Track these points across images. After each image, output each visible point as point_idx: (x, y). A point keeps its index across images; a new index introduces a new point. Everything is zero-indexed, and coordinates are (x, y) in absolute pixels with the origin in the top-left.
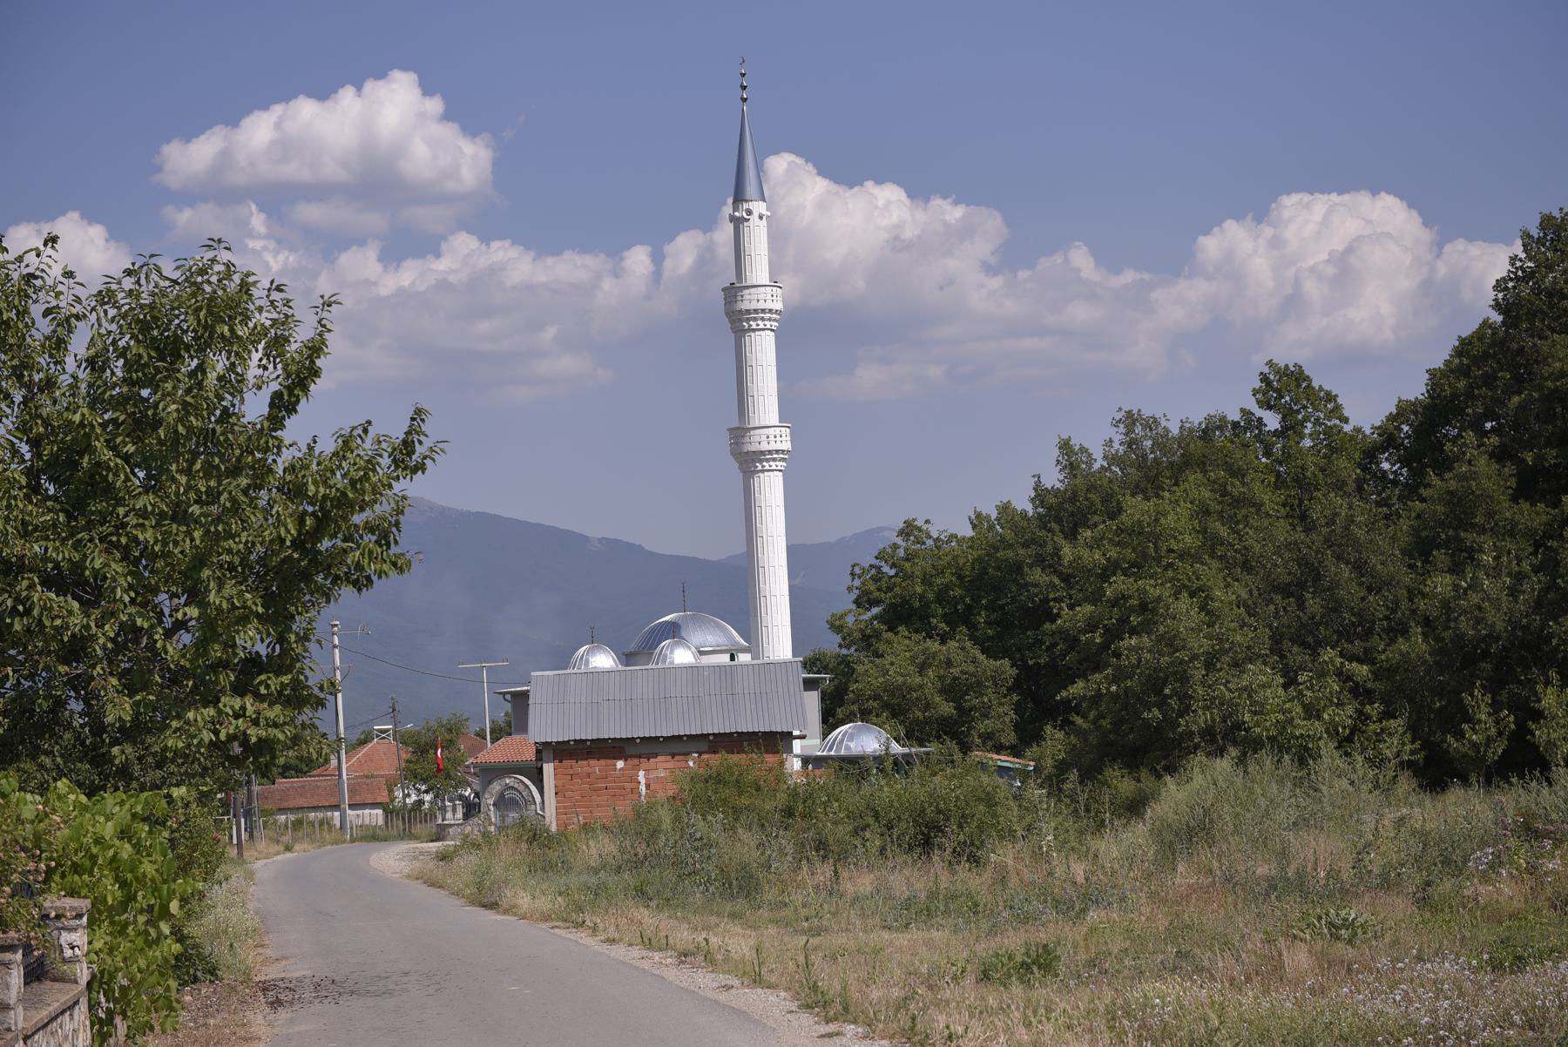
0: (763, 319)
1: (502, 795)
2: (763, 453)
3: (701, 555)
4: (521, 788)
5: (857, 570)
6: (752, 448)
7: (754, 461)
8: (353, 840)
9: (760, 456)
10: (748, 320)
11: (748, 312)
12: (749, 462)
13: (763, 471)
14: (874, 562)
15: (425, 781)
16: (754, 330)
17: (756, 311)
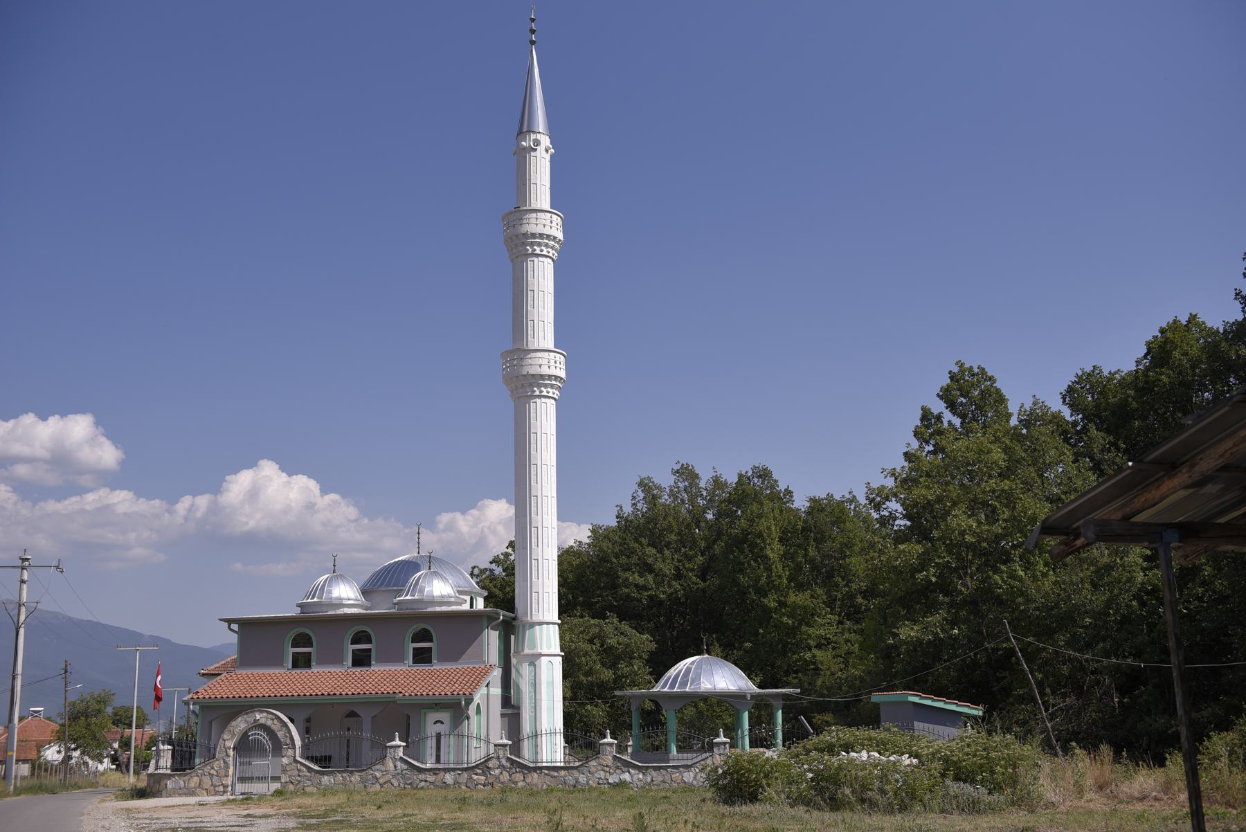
0: (547, 246)
1: (245, 735)
2: (542, 377)
3: (200, 645)
4: (275, 726)
5: (476, 571)
6: (533, 370)
7: (531, 385)
8: (18, 792)
9: (539, 379)
10: (532, 244)
11: (534, 236)
12: (524, 387)
13: (540, 397)
14: (488, 566)
15: (75, 741)
16: (537, 256)
17: (541, 236)
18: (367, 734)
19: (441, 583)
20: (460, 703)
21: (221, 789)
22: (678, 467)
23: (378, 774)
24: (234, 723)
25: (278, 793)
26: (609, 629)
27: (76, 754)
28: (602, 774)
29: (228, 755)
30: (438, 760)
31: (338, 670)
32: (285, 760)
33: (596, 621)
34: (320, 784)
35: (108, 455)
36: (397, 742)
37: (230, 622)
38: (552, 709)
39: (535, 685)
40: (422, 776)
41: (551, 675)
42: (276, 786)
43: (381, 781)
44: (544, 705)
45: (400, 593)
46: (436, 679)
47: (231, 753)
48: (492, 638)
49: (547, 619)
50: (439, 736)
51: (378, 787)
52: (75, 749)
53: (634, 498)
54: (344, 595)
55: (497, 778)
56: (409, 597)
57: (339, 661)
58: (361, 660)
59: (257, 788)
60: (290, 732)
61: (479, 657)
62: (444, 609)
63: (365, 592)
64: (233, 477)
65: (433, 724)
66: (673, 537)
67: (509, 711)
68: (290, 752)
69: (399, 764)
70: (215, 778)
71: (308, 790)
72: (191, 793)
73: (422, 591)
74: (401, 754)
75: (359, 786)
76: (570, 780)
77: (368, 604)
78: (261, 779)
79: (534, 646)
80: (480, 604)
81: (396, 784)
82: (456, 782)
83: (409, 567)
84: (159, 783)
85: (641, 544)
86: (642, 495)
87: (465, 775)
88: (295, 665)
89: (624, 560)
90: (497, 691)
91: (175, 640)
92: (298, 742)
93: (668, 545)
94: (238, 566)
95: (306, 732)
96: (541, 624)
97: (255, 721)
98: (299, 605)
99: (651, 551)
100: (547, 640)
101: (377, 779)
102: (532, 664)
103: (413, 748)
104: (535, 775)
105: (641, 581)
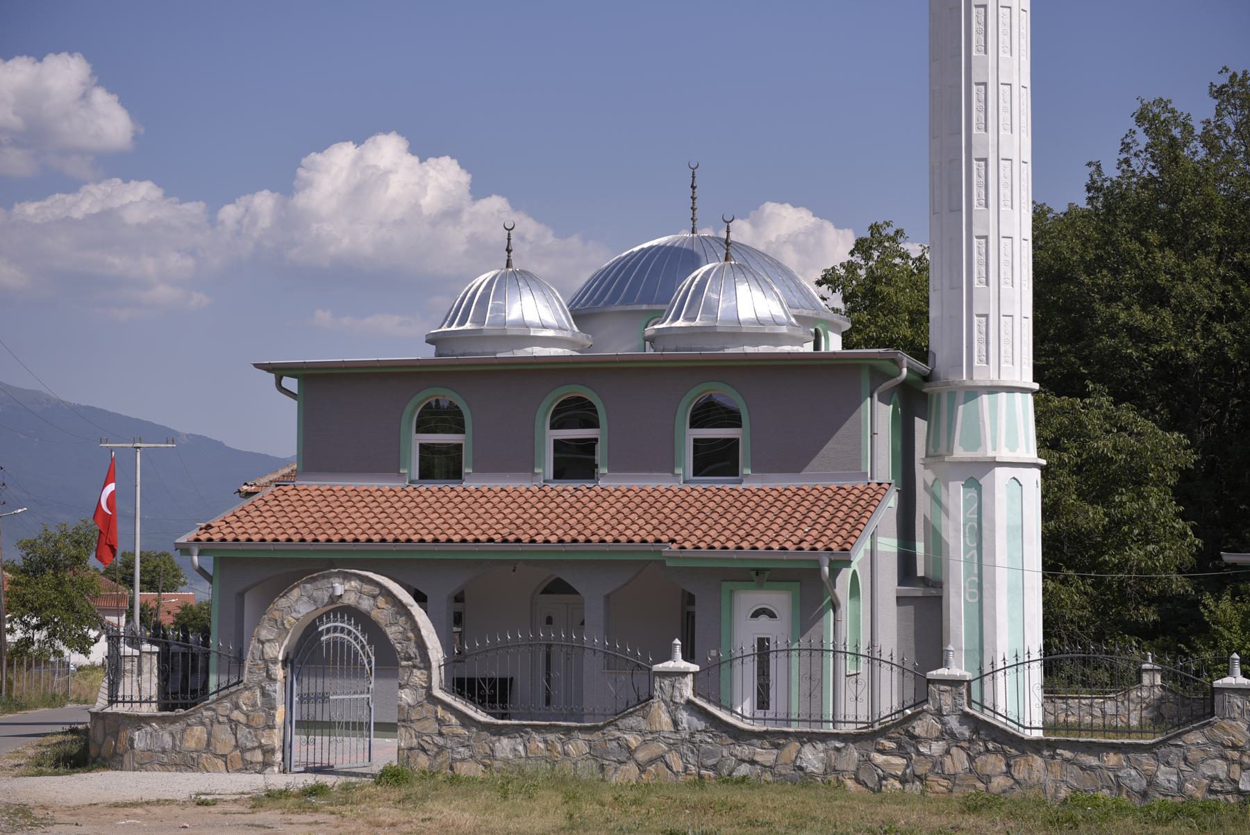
1: (310, 633)
4: (382, 613)
15: (36, 611)
18: (594, 638)
19: (758, 294)
20: (818, 571)
21: (258, 756)
22: (1224, 80)
23: (633, 740)
24: (282, 602)
25: (391, 777)
26: (1093, 421)
27: (40, 635)
28: (1221, 768)
29: (271, 679)
30: (763, 703)
31: (523, 485)
32: (406, 696)
33: (1065, 401)
34: (492, 756)
35: (112, 122)
36: (678, 663)
37: (280, 371)
38: (1020, 590)
39: (979, 533)
40: (743, 750)
41: (1011, 517)
42: (386, 751)
43: (641, 756)
44: (1002, 578)
45: (659, 316)
46: (754, 509)
47: (279, 672)
48: (879, 417)
49: (1008, 379)
50: (763, 649)
51: (631, 770)
52: (38, 627)
53: (1126, 147)
54: (531, 317)
55: (937, 764)
56: (680, 323)
57: (523, 464)
58: (575, 463)
59: (347, 752)
60: (416, 628)
61: (853, 463)
62: (763, 349)
63: (581, 313)
64: (315, 157)
65: (750, 620)
66: (1217, 229)
67: (918, 591)
68: (418, 676)
69: (684, 716)
70: (243, 732)
71: (464, 769)
72: (189, 763)
73: (711, 309)
74: (688, 693)
75: (587, 769)
76: (1133, 778)
77: (585, 339)
78: (357, 727)
79: (976, 439)
80: (834, 343)
81: (678, 765)
82: (830, 769)
83: (679, 260)
84: (116, 735)
85: (1144, 242)
86: (1143, 139)
87: (853, 753)
88: (426, 473)
89: (1105, 277)
90: (889, 545)
91: (230, 443)
92: (436, 653)
93: (1203, 245)
94: (323, 317)
95: (455, 622)
96: (994, 390)
97: (334, 599)
98: (432, 340)
99: (1169, 258)
100: (1008, 427)
101: (631, 752)
102: (973, 483)
103: (712, 683)
104: (1038, 762)
105: (1144, 320)
